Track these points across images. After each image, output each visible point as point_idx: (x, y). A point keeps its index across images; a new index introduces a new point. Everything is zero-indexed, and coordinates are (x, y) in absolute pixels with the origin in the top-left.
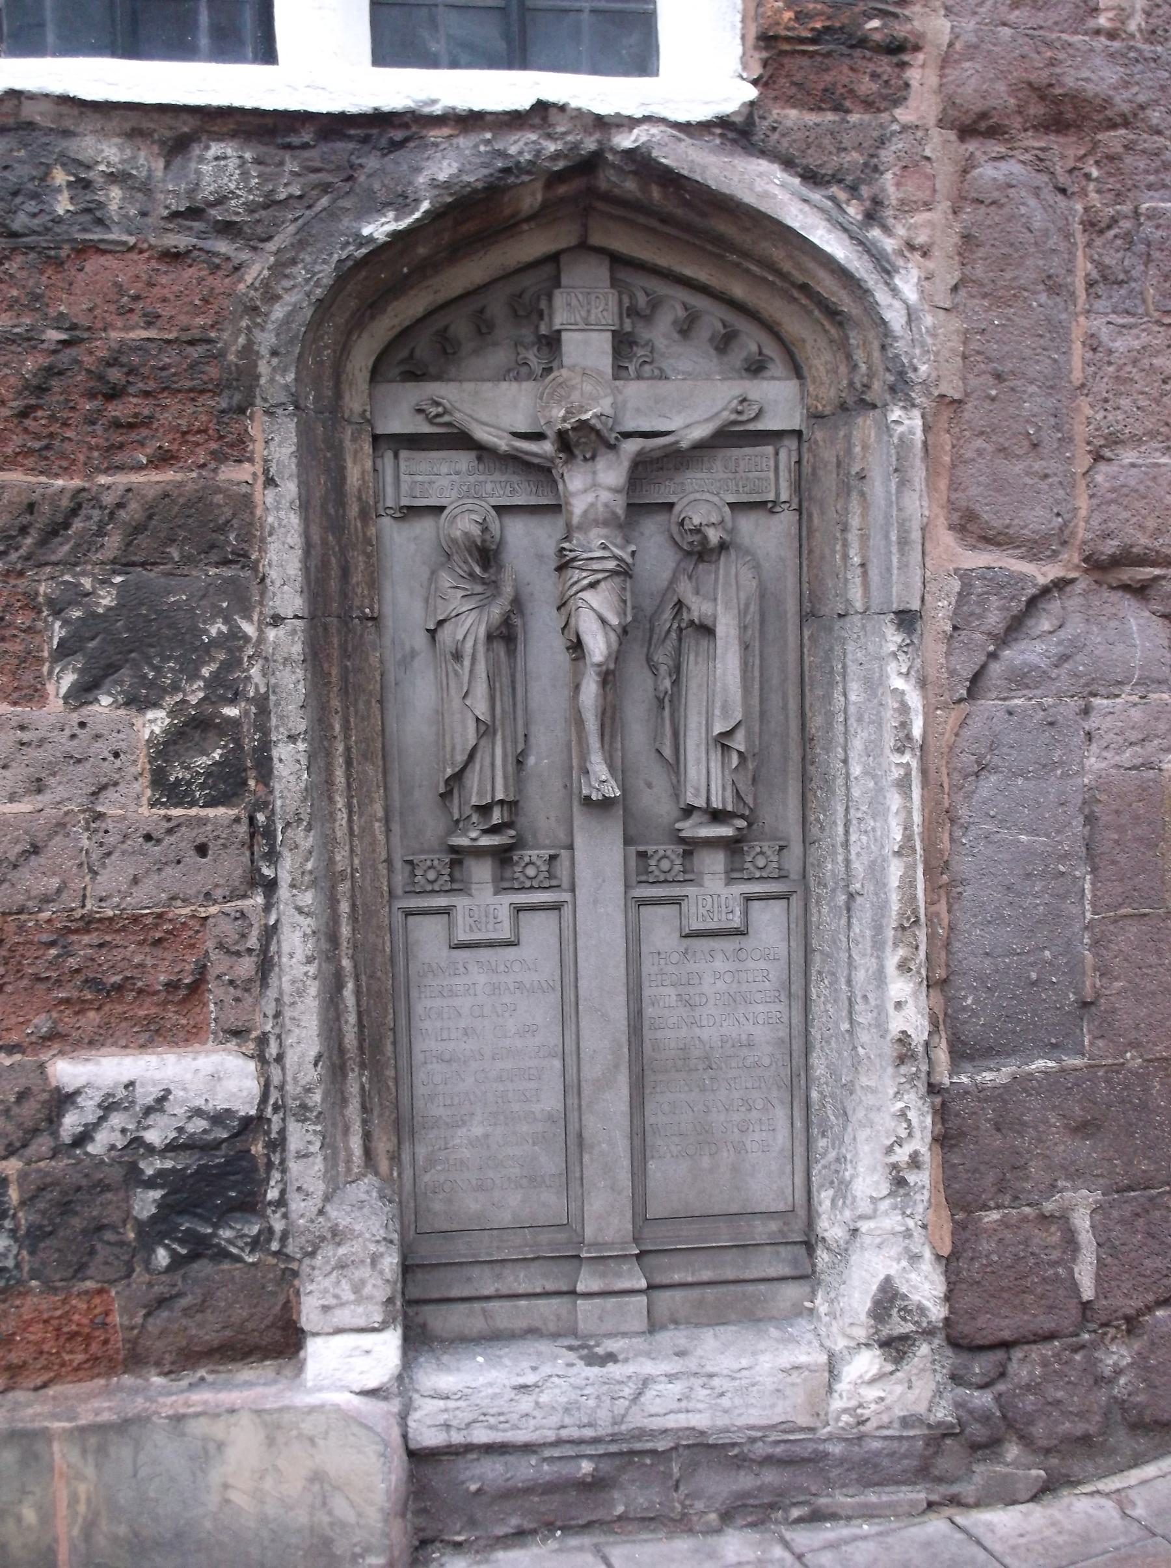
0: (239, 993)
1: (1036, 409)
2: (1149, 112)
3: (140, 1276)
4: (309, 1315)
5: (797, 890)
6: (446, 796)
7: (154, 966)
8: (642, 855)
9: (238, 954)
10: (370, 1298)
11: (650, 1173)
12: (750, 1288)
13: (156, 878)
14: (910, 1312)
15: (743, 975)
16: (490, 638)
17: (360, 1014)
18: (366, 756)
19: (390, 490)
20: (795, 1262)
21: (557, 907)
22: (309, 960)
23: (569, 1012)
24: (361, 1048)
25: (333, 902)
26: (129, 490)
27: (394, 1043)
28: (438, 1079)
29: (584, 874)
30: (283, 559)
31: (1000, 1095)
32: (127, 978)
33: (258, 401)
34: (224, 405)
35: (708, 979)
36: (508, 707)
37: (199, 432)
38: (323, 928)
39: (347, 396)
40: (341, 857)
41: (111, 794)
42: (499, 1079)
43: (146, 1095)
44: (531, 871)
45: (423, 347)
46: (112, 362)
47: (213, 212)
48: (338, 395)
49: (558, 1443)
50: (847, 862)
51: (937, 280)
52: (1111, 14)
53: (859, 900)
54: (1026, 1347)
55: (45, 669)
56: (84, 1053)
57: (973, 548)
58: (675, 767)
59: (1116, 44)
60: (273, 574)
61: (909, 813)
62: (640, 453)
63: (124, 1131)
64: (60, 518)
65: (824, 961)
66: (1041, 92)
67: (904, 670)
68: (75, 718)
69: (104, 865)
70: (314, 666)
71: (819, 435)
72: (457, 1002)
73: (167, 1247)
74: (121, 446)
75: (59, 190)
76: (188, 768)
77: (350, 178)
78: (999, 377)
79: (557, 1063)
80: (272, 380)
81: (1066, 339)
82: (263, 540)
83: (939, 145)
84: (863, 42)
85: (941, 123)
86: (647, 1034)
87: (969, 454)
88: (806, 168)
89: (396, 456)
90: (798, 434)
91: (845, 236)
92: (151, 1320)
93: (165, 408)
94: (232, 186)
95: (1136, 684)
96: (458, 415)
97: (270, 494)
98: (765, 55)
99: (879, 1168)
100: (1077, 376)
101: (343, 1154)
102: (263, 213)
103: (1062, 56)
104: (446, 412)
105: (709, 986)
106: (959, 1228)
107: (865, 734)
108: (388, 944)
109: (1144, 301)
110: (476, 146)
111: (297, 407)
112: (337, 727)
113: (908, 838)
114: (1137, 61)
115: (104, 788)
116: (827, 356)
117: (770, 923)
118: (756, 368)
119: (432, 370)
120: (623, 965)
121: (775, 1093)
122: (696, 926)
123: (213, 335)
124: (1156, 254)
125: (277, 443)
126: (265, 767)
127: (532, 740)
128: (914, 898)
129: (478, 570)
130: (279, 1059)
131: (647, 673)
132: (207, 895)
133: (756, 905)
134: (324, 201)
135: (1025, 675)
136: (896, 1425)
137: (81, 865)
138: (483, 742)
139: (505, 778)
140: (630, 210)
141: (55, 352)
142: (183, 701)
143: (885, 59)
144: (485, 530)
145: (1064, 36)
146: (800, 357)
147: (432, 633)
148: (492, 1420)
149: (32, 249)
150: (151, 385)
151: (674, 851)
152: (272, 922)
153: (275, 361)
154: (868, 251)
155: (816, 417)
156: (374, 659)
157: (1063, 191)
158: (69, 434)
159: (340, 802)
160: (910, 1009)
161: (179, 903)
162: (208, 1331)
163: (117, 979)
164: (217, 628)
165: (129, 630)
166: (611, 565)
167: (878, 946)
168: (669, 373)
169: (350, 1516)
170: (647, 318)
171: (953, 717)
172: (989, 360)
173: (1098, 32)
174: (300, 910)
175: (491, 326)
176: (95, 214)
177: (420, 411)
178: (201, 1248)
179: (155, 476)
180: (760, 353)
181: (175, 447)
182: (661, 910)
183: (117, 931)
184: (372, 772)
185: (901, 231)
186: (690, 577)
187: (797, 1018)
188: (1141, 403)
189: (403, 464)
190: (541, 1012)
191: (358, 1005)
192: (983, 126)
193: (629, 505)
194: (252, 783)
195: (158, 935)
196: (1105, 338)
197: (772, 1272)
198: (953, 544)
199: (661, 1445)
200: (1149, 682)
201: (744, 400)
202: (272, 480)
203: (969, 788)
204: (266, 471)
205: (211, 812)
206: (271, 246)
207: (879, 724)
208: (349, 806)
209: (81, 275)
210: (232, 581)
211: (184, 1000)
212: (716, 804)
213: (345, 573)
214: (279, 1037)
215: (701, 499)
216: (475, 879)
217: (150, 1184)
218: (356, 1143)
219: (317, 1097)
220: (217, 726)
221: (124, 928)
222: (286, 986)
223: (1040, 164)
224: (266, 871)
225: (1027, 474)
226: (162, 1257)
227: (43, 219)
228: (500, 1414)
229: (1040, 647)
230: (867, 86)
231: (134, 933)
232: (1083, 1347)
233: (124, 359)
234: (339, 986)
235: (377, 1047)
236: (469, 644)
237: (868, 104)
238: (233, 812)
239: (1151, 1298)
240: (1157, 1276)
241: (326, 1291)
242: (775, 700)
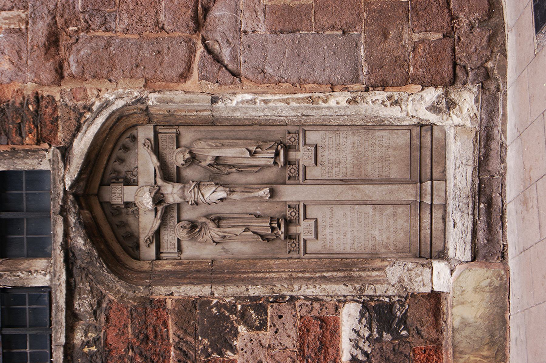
0: (324, 308)
1: (147, 52)
2: (50, 9)
3: (410, 339)
4: (427, 290)
5: (302, 127)
6: (268, 240)
7: (315, 332)
8: (289, 178)
9: (312, 307)
10: (421, 272)
11: (395, 177)
12: (434, 146)
13: (288, 330)
14: (439, 101)
15: (330, 146)
16: (218, 227)
17: (334, 271)
18: (255, 265)
19: (173, 255)
20: (427, 131)
21: (305, 206)
22: (315, 287)
23: (341, 204)
24: (343, 271)
25: (298, 278)
26: (174, 334)
27: (347, 259)
28: (360, 245)
29: (294, 198)
30: (194, 291)
31: (371, 67)
32: (318, 340)
33: (148, 297)
34: (149, 306)
35: (331, 157)
36: (241, 220)
37: (157, 314)
38: (306, 282)
39: (145, 269)
40: (284, 275)
41: (263, 342)
42: (361, 226)
43: (354, 336)
44: (293, 214)
45: (129, 244)
46: (138, 337)
47: (94, 308)
48: (145, 272)
49: (473, 214)
50: (291, 116)
51: (108, 87)
52: (21, 24)
53: (304, 113)
54: (456, 59)
55: (226, 359)
56: (341, 353)
57: (192, 73)
58: (262, 168)
59: (30, 22)
60: (199, 294)
61: (275, 100)
62: (161, 178)
63: (364, 343)
64: (182, 354)
65: (325, 121)
66: (47, 49)
67: (230, 101)
68: (240, 352)
69: (284, 345)
70: (226, 283)
72: (335, 238)
73: (401, 331)
74: (162, 336)
75: (90, 350)
76: (256, 320)
77: (83, 268)
78: (137, 66)
79: (357, 207)
80: (142, 293)
81: (124, 40)
82: (189, 297)
83: (67, 87)
84: (36, 111)
85: (60, 85)
86: (348, 177)
87: (162, 76)
88: (75, 130)
89: (162, 253)
90: (155, 126)
91: (96, 119)
92: (424, 337)
93: (151, 323)
94: (87, 302)
95: (237, 15)
96: (150, 234)
97: (175, 294)
98: (42, 142)
99: (391, 109)
100: (137, 37)
101: (377, 278)
102: (94, 294)
103: (35, 42)
104: (149, 238)
105: (334, 157)
106: (414, 82)
107: (251, 111)
108: (314, 260)
109: (112, 12)
110: (73, 232)
111: (150, 286)
112: (245, 276)
113: (283, 100)
114: (34, 14)
115: (261, 344)
116: (131, 119)
117: (313, 137)
118: (134, 139)
119: (135, 240)
120: (324, 186)
121: (370, 136)
122: (313, 161)
123: (129, 309)
124: (96, 7)
125: (160, 292)
126: (258, 298)
127: (252, 212)
128: (303, 99)
129: (197, 230)
130: (345, 296)
131: (231, 175)
132: (294, 316)
133: (307, 141)
134: (90, 276)
135: (233, 56)
136: (477, 104)
137: (284, 352)
138: (251, 230)
139: (261, 222)
140: (89, 182)
141: (135, 353)
142: (236, 321)
143: (41, 103)
144: (185, 227)
145: (29, 41)
146: (130, 125)
147: (217, 243)
148: (464, 235)
149: (106, 358)
150: (144, 327)
151: (288, 168)
152: (303, 297)
153: (137, 292)
154: (101, 111)
155: (150, 121)
156: (224, 262)
157: (77, 40)
158: (158, 350)
159: (268, 275)
160: (339, 99)
161: (296, 325)
162: (429, 319)
163: (318, 343)
164: (214, 310)
165: (215, 336)
166: (196, 189)
167: (319, 108)
168: (135, 166)
169: (488, 281)
170: (119, 172)
171: (245, 82)
172: (132, 69)
173: (27, 28)
174: (299, 289)
175: (122, 222)
176: (96, 341)
177: (149, 246)
178: (403, 320)
179: (170, 326)
180: (129, 138)
181: (162, 321)
182: (308, 172)
183: (304, 342)
184: (260, 264)
185: (93, 99)
186: (200, 162)
187: (345, 128)
188: (145, 13)
189: (164, 251)
190: (339, 211)
191: (331, 271)
192: (59, 71)
193: (177, 182)
194: (261, 302)
195: (306, 331)
196: (124, 27)
197: (429, 139)
198: (190, 81)
199: (477, 181)
200: (237, 10)
201: (144, 144)
203: (269, 77)
204: (169, 295)
205: (269, 314)
206: (104, 292)
207: (247, 108)
208: (269, 272)
209: (113, 345)
210: (200, 305)
211: (326, 324)
212: (273, 156)
213: (198, 271)
214: (338, 297)
215: (177, 158)
216: (295, 232)
217: (381, 336)
218: (374, 274)
219: (357, 286)
220: (243, 312)
221: (303, 340)
222: (322, 294)
223: (69, 48)
224: (287, 299)
225: (168, 55)
226: (404, 333)
227: (98, 354)
228: (462, 233)
229: (224, 50)
230: (49, 110)
231: (305, 337)
232: (459, 38)
233: (137, 334)
234: (325, 277)
235: (347, 265)
236: (220, 234)
237: (55, 109)
238: (269, 308)
239: (446, 11)
240: (439, 8)
241: (418, 285)
242: (241, 134)
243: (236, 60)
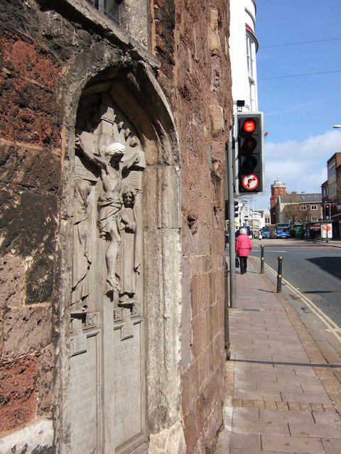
33: (64, 123)
71: (148, 170)
164: (48, 219)
167: (174, 334)
202: (68, 157)
238: (49, 304)
243: (228, 245)
